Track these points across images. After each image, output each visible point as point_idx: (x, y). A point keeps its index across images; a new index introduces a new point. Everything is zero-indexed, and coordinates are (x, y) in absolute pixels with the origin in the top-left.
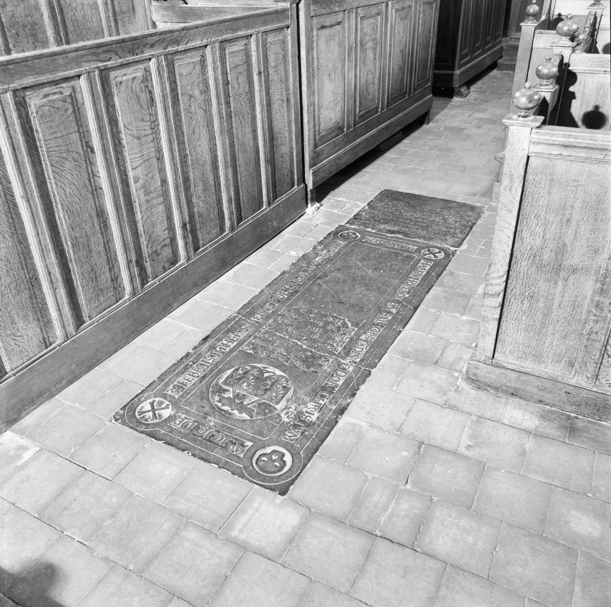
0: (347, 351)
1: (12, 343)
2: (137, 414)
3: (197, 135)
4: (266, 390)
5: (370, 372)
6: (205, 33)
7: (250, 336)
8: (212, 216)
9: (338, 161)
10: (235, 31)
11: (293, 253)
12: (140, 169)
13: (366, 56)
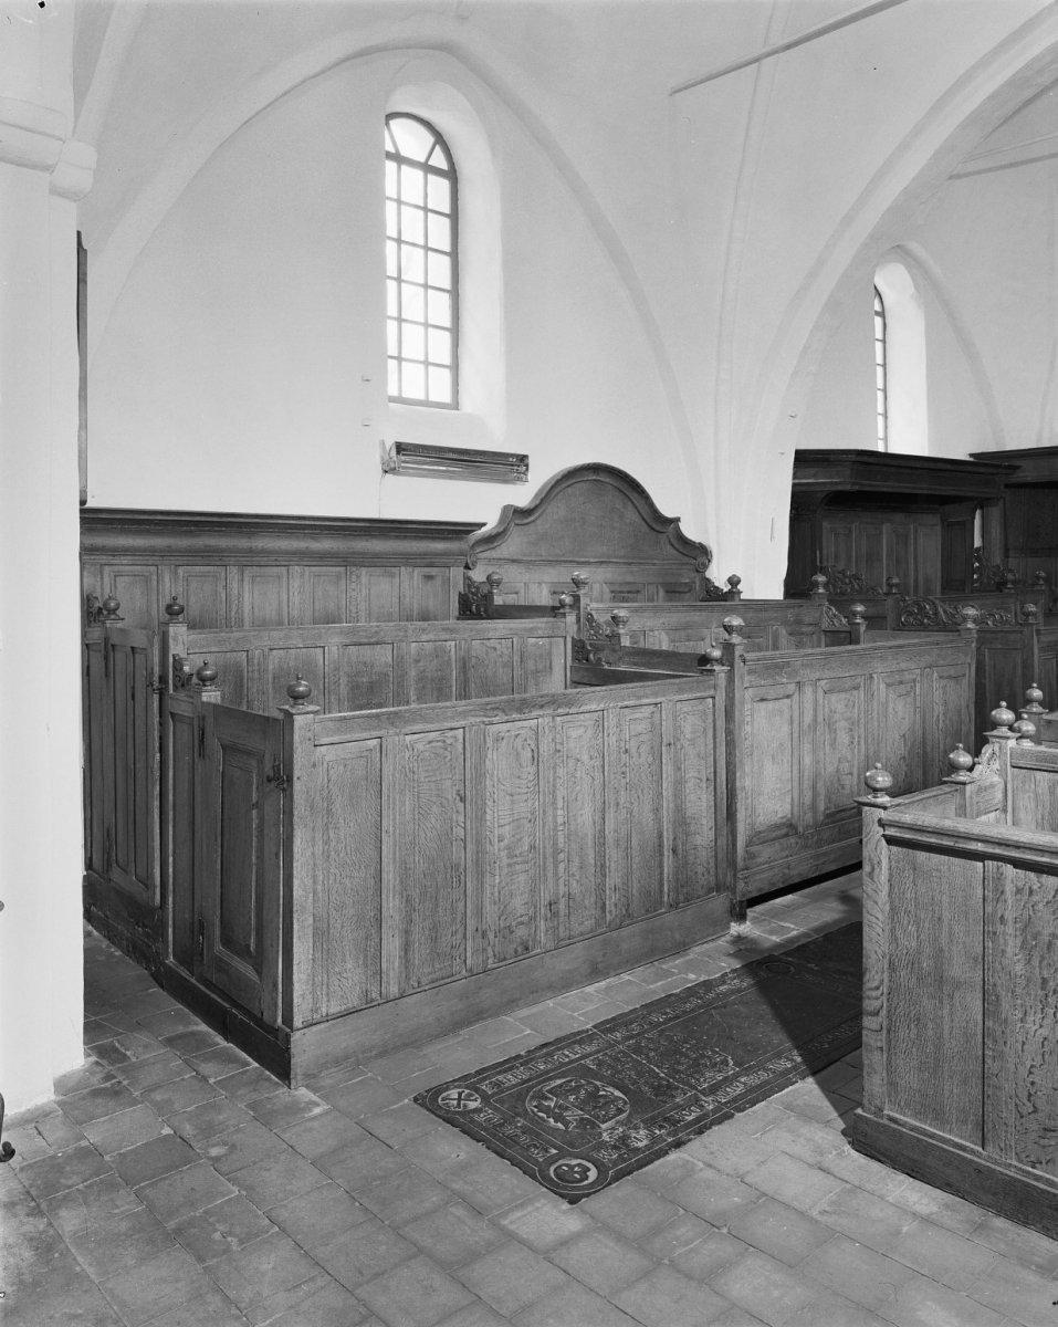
0: (713, 1090)
1: (336, 983)
2: (440, 1099)
3: (579, 803)
4: (596, 1107)
5: (733, 1115)
6: (603, 698)
7: (599, 1052)
8: (587, 902)
9: (786, 871)
10: (639, 698)
11: (692, 976)
12: (507, 827)
13: (835, 739)
